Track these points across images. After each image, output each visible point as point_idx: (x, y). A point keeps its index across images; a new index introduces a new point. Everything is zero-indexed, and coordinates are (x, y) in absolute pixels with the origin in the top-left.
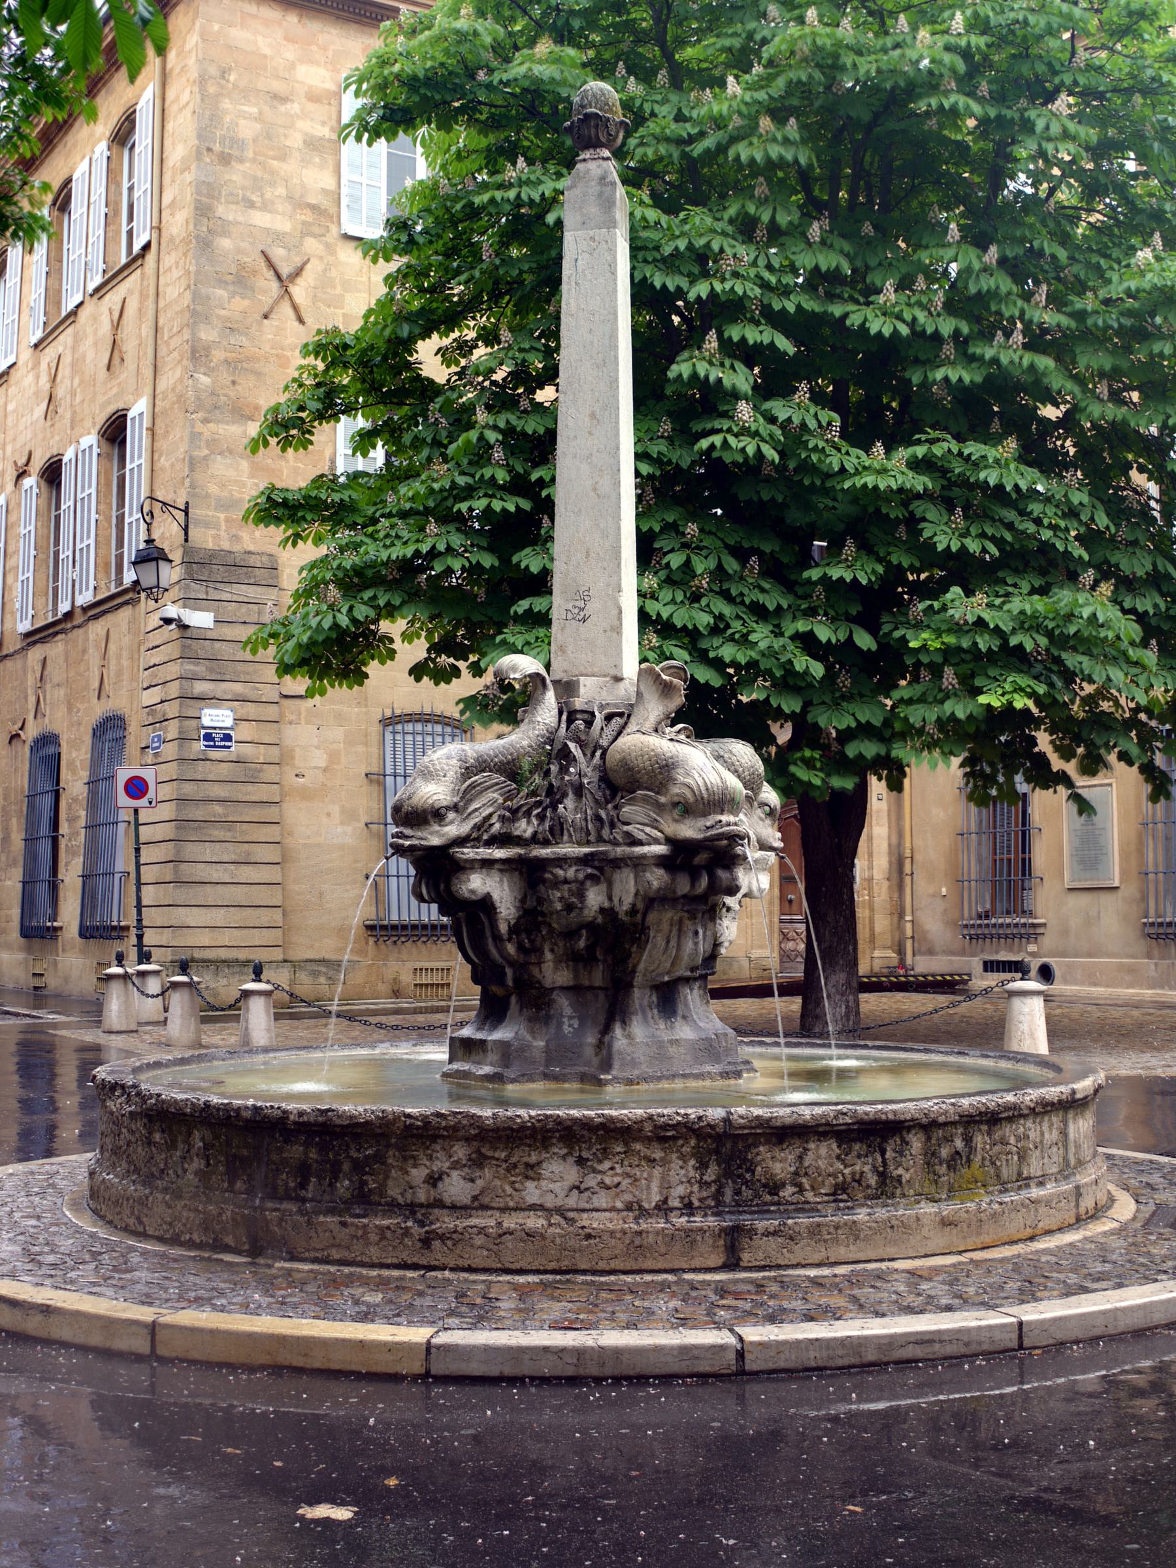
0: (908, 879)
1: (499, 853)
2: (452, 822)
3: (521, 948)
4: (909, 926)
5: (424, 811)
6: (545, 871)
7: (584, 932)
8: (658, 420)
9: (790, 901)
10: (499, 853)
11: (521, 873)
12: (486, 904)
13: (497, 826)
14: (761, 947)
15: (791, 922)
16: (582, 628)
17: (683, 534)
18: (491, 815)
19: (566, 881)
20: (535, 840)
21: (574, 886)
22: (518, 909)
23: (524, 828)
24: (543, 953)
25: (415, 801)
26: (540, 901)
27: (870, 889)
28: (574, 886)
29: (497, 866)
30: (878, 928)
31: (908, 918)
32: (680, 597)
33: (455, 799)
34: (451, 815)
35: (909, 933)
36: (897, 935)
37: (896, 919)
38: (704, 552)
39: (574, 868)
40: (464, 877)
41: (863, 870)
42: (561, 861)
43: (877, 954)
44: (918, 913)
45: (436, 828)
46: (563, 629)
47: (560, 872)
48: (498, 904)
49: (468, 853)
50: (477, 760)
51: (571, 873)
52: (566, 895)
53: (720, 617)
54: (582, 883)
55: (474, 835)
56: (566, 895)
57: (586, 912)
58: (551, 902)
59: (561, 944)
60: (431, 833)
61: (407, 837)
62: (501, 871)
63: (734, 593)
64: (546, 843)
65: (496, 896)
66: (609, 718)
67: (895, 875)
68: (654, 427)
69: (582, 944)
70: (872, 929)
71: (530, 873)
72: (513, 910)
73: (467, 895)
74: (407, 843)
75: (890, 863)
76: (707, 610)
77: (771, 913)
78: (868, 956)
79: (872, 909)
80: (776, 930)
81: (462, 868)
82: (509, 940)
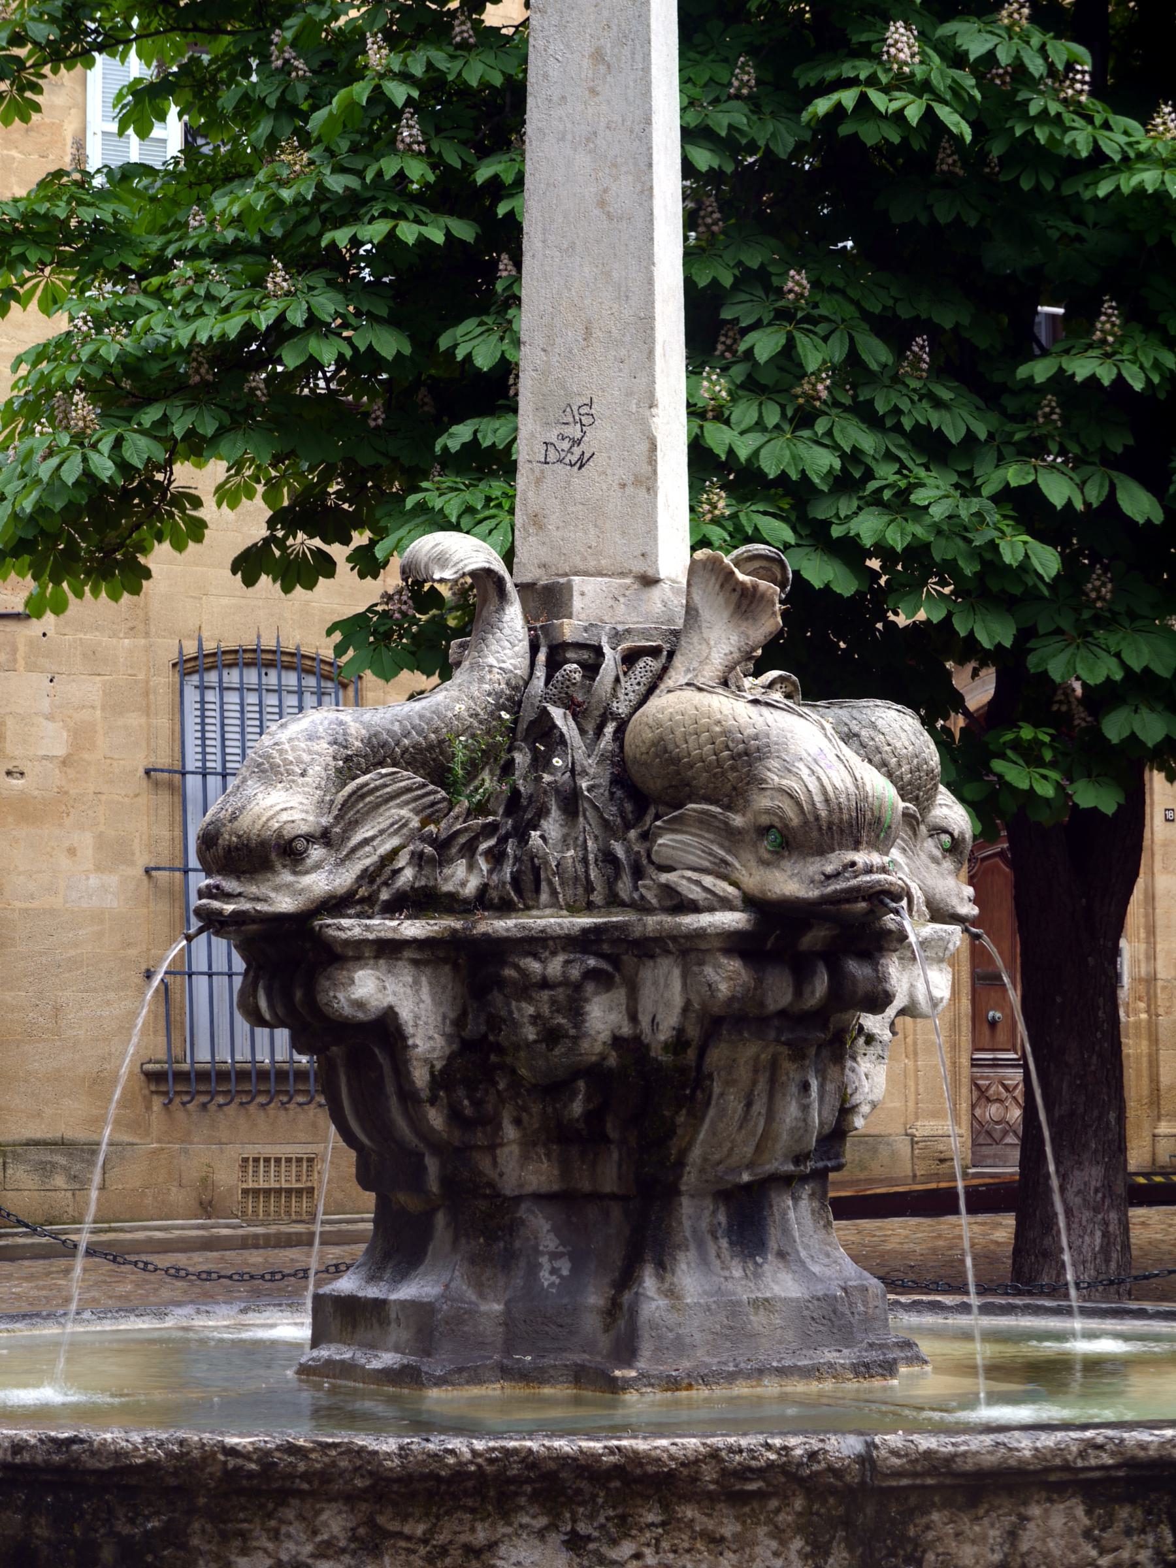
1: (412, 928)
2: (317, 866)
3: (455, 1116)
5: (263, 844)
6: (504, 963)
7: (581, 1084)
9: (993, 1024)
10: (412, 928)
11: (456, 967)
12: (386, 1029)
13: (408, 874)
14: (935, 1114)
15: (995, 1064)
16: (578, 479)
17: (780, 293)
18: (395, 852)
19: (545, 983)
20: (483, 901)
21: (561, 993)
22: (449, 1038)
23: (463, 878)
24: (499, 1127)
25: (245, 823)
28: (561, 993)
29: (407, 954)
32: (772, 417)
33: (325, 821)
34: (316, 853)
38: (821, 329)
39: (561, 958)
41: (1135, 962)
42: (537, 944)
45: (287, 877)
46: (539, 481)
47: (535, 966)
48: (410, 1030)
49: (350, 927)
50: (368, 742)
51: (555, 967)
52: (546, 1010)
53: (854, 456)
54: (578, 987)
56: (546, 1010)
57: (585, 1045)
58: (515, 1025)
59: (536, 1109)
60: (277, 889)
61: (227, 896)
62: (416, 963)
63: (881, 407)
64: (505, 908)
65: (405, 1013)
66: (630, 658)
69: (577, 1108)
70: (1154, 1079)
71: (472, 968)
72: (440, 1041)
73: (348, 1011)
74: (229, 908)
76: (828, 442)
77: (954, 1047)
80: (965, 1081)
82: (433, 1101)
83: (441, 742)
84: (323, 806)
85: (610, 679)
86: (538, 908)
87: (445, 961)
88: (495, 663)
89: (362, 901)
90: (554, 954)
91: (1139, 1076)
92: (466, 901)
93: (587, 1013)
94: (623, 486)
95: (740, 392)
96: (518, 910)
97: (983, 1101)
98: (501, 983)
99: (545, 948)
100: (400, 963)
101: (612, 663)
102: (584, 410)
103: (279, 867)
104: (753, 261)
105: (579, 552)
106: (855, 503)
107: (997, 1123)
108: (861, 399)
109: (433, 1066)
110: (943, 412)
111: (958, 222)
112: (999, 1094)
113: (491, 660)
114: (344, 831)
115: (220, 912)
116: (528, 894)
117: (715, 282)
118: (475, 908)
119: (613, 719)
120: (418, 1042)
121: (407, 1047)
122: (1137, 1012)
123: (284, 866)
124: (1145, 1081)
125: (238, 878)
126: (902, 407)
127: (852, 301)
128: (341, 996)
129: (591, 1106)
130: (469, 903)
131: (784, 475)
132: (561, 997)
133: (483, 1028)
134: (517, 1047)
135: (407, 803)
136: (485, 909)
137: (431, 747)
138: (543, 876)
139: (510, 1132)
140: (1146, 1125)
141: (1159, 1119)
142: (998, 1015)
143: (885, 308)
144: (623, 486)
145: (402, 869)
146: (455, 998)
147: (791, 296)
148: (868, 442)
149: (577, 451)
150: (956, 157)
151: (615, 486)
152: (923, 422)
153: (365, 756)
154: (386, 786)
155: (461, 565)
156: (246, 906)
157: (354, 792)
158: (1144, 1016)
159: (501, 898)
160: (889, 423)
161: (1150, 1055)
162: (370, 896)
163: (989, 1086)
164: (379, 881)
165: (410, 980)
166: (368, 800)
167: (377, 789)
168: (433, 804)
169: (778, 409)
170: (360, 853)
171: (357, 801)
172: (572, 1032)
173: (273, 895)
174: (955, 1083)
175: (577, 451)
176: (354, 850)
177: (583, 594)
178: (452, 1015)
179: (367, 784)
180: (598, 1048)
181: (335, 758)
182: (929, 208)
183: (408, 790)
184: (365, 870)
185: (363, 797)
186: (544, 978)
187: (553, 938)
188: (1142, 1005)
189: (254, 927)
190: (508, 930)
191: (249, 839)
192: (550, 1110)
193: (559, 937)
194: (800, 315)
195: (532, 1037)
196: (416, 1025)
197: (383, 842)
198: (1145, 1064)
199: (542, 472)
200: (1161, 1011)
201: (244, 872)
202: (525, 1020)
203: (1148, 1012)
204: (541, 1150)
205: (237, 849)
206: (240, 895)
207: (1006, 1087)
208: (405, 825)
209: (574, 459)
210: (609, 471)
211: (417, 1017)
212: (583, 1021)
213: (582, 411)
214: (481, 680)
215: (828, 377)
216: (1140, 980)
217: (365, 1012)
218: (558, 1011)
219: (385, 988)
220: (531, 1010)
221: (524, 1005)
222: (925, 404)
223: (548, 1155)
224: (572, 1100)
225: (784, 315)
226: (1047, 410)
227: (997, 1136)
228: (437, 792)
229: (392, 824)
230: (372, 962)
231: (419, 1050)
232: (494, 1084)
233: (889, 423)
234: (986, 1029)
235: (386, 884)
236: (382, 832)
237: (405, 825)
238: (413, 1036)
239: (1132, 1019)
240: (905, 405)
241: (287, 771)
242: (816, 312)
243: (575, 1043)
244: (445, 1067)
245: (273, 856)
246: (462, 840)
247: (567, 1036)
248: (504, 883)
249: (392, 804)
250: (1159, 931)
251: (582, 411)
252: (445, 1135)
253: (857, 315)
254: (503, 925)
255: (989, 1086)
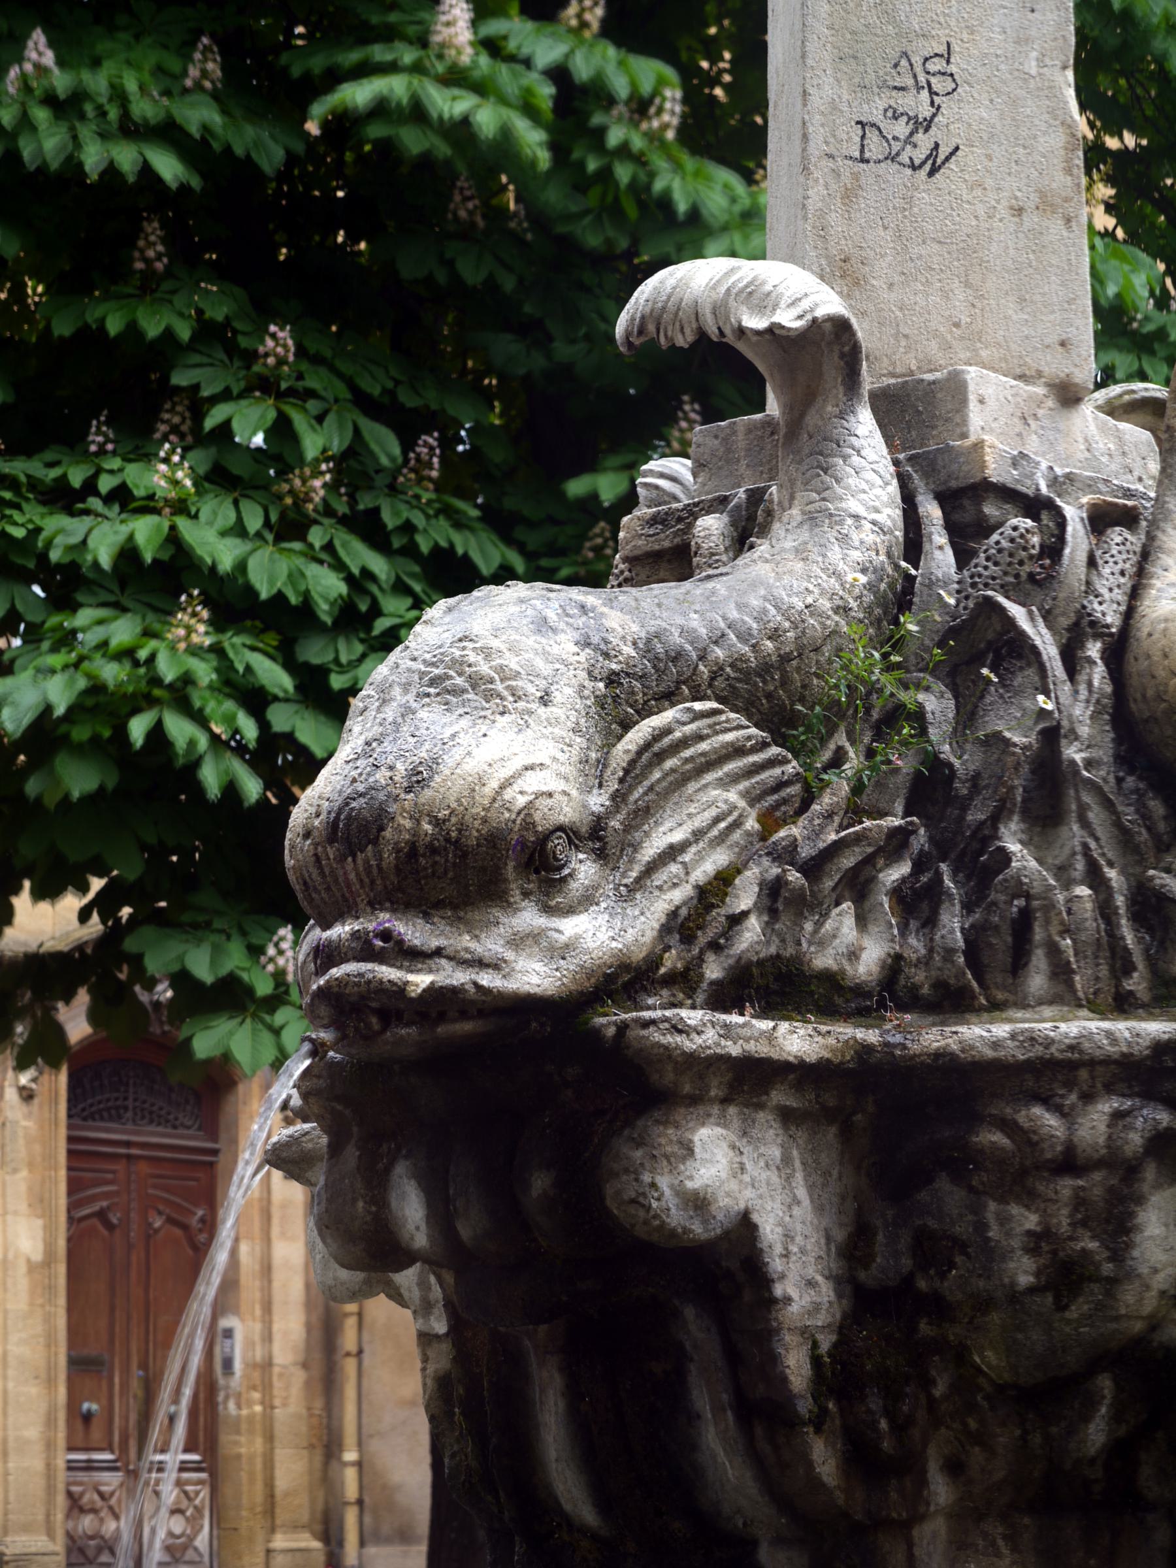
0: (350, 1365)
1: (797, 1040)
2: (587, 901)
3: (859, 1456)
4: (351, 1475)
5: (494, 839)
6: (976, 1119)
7: (1105, 1384)
8: (185, 49)
9: (87, 1418)
10: (797, 1040)
11: (847, 1132)
12: (730, 1265)
13: (752, 933)
14: (26, 1528)
15: (89, 1466)
16: (928, 194)
17: (251, 356)
18: (724, 880)
19: (1070, 1162)
20: (893, 991)
21: (1096, 1183)
22: (837, 1281)
23: (853, 944)
24: (922, 1482)
25: (446, 789)
26: (933, 1250)
27: (266, 1387)
28: (1096, 1183)
29: (779, 1096)
30: (282, 1482)
31: (350, 1456)
32: (254, 523)
33: (598, 801)
34: (584, 869)
35: (351, 1490)
36: (320, 1495)
37: (318, 1459)
38: (313, 406)
39: (1106, 1106)
40: (666, 1138)
41: (249, 1344)
42: (1054, 1074)
43: (280, 1542)
44: (374, 1445)
45: (529, 917)
46: (849, 195)
47: (1049, 1122)
48: (776, 1265)
49: (703, 1029)
50: (646, 648)
51: (1094, 1123)
52: (1062, 1221)
53: (359, 582)
54: (1130, 1170)
55: (672, 961)
56: (1062, 1221)
57: (1128, 1296)
58: (989, 1255)
59: (1004, 1438)
60: (518, 942)
61: (414, 956)
62: (787, 1117)
63: (390, 520)
64: (951, 1002)
65: (769, 1229)
66: (1103, 519)
67: (318, 1355)
68: (174, 65)
69: (1096, 1434)
70: (270, 1484)
71: (894, 1132)
72: (826, 1292)
73: (676, 1217)
74: (420, 981)
75: (309, 1327)
76: (330, 555)
77: (49, 1445)
78: (260, 1550)
79: (270, 1438)
80: (61, 1487)
81: (650, 1090)
82: (819, 1422)
83: (785, 659)
84: (594, 771)
85: (1082, 557)
86: (1025, 1006)
87: (828, 1115)
88: (862, 512)
89: (671, 980)
90: (1088, 1097)
91: (252, 1481)
92: (859, 991)
93: (1137, 1229)
94: (1019, 211)
95: (207, 485)
96: (978, 1010)
97: (76, 1511)
98: (962, 1163)
99: (1070, 1085)
100: (761, 1116)
101: (1079, 527)
102: (935, 65)
103: (516, 896)
104: (218, 313)
105: (936, 334)
106: (359, 648)
107: (92, 1538)
108: (361, 507)
109: (815, 1345)
110: (468, 533)
111: (491, 284)
112: (93, 1502)
113: (853, 505)
114: (628, 828)
115: (399, 991)
116: (996, 977)
117: (169, 334)
118: (882, 1005)
119: (1097, 636)
120: (793, 1292)
121: (773, 1301)
122: (250, 1404)
123: (526, 894)
124: (259, 1486)
125: (427, 916)
126: (415, 521)
127: (340, 375)
128: (664, 1182)
129: (1122, 1431)
130: (868, 995)
131: (280, 597)
132: (1097, 1192)
133: (907, 1263)
134: (984, 1304)
135: (734, 778)
136: (902, 1007)
137: (765, 669)
138: (1038, 934)
139: (941, 1491)
140: (260, 1536)
141: (273, 1530)
142: (95, 1407)
143: (385, 391)
144: (1019, 211)
145: (745, 914)
146: (843, 1198)
147: (271, 361)
148: (379, 565)
149: (924, 142)
150: (477, 202)
151: (1003, 211)
152: (443, 544)
153: (642, 677)
154: (699, 738)
155: (805, 304)
156: (459, 977)
157: (647, 746)
158: (258, 1408)
159: (940, 985)
160: (397, 543)
161: (264, 1455)
162: (687, 969)
163: (82, 1494)
164: (703, 939)
165: (776, 1153)
166: (669, 764)
167: (684, 743)
168: (780, 785)
169: (259, 511)
170: (660, 877)
171: (650, 766)
172: (1108, 1269)
173: (510, 955)
174: (50, 1489)
175: (924, 142)
176: (651, 868)
177: (981, 401)
178: (840, 1235)
179: (667, 731)
180: (1150, 1304)
181: (591, 676)
182: (450, 264)
183: (737, 751)
184: (673, 914)
185: (660, 757)
186: (1070, 1148)
187: (1092, 1063)
188: (256, 1395)
189: (466, 1027)
190: (996, 1044)
191: (462, 828)
192: (1037, 1439)
193: (1107, 1061)
194: (284, 385)
195: (1025, 1280)
196: (786, 1255)
197: (700, 858)
198: (259, 1466)
199: (856, 177)
200: (277, 1402)
201: (439, 905)
202: (1016, 1243)
203: (262, 1403)
204: (997, 1530)
205: (433, 850)
206: (438, 952)
207: (102, 1495)
208: (737, 824)
209: (919, 155)
210: (989, 182)
211: (788, 1237)
212: (1129, 1246)
213: (931, 67)
214: (844, 539)
215: (329, 471)
216: (255, 1366)
217: (705, 1222)
218: (1084, 1223)
219: (742, 1169)
220: (1032, 1221)
221: (1015, 1210)
222: (442, 522)
223: (1012, 1539)
224: (1086, 1419)
225: (266, 386)
226: (599, 541)
227: (90, 1553)
228: (785, 761)
229: (717, 820)
230: (715, 1110)
231: (794, 1308)
232: (927, 1383)
233: (397, 543)
234: (79, 1425)
235: (715, 947)
236: (698, 834)
237: (737, 824)
238: (783, 1277)
239: (244, 1412)
240: (419, 520)
241: (513, 691)
242: (300, 385)
243: (1109, 1294)
244: (835, 1346)
245: (510, 870)
246: (848, 861)
247: (1095, 1278)
248: (950, 952)
249: (710, 777)
250: (276, 1308)
251: (931, 67)
252: (840, 1498)
253: (349, 396)
254: (981, 1034)
255: (82, 1494)
